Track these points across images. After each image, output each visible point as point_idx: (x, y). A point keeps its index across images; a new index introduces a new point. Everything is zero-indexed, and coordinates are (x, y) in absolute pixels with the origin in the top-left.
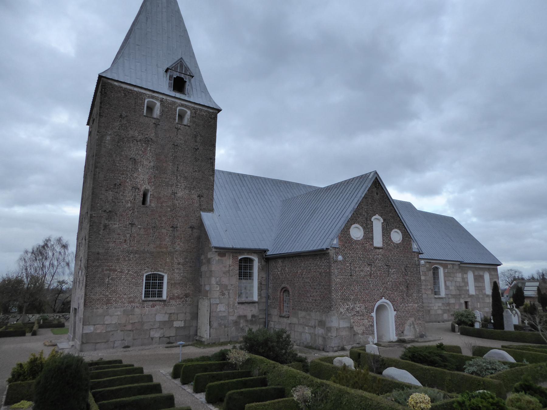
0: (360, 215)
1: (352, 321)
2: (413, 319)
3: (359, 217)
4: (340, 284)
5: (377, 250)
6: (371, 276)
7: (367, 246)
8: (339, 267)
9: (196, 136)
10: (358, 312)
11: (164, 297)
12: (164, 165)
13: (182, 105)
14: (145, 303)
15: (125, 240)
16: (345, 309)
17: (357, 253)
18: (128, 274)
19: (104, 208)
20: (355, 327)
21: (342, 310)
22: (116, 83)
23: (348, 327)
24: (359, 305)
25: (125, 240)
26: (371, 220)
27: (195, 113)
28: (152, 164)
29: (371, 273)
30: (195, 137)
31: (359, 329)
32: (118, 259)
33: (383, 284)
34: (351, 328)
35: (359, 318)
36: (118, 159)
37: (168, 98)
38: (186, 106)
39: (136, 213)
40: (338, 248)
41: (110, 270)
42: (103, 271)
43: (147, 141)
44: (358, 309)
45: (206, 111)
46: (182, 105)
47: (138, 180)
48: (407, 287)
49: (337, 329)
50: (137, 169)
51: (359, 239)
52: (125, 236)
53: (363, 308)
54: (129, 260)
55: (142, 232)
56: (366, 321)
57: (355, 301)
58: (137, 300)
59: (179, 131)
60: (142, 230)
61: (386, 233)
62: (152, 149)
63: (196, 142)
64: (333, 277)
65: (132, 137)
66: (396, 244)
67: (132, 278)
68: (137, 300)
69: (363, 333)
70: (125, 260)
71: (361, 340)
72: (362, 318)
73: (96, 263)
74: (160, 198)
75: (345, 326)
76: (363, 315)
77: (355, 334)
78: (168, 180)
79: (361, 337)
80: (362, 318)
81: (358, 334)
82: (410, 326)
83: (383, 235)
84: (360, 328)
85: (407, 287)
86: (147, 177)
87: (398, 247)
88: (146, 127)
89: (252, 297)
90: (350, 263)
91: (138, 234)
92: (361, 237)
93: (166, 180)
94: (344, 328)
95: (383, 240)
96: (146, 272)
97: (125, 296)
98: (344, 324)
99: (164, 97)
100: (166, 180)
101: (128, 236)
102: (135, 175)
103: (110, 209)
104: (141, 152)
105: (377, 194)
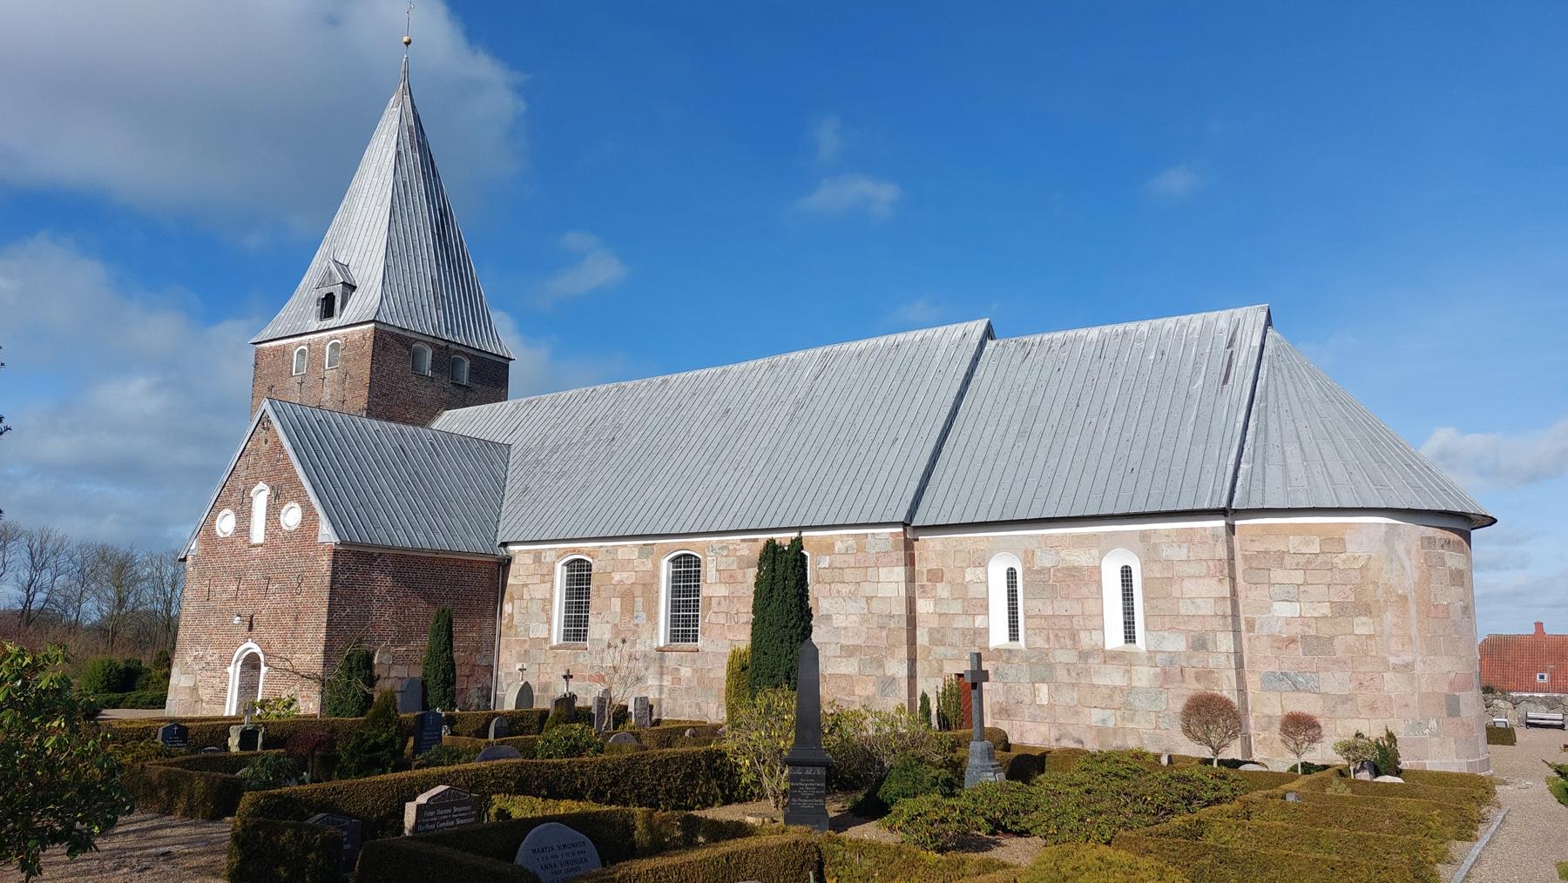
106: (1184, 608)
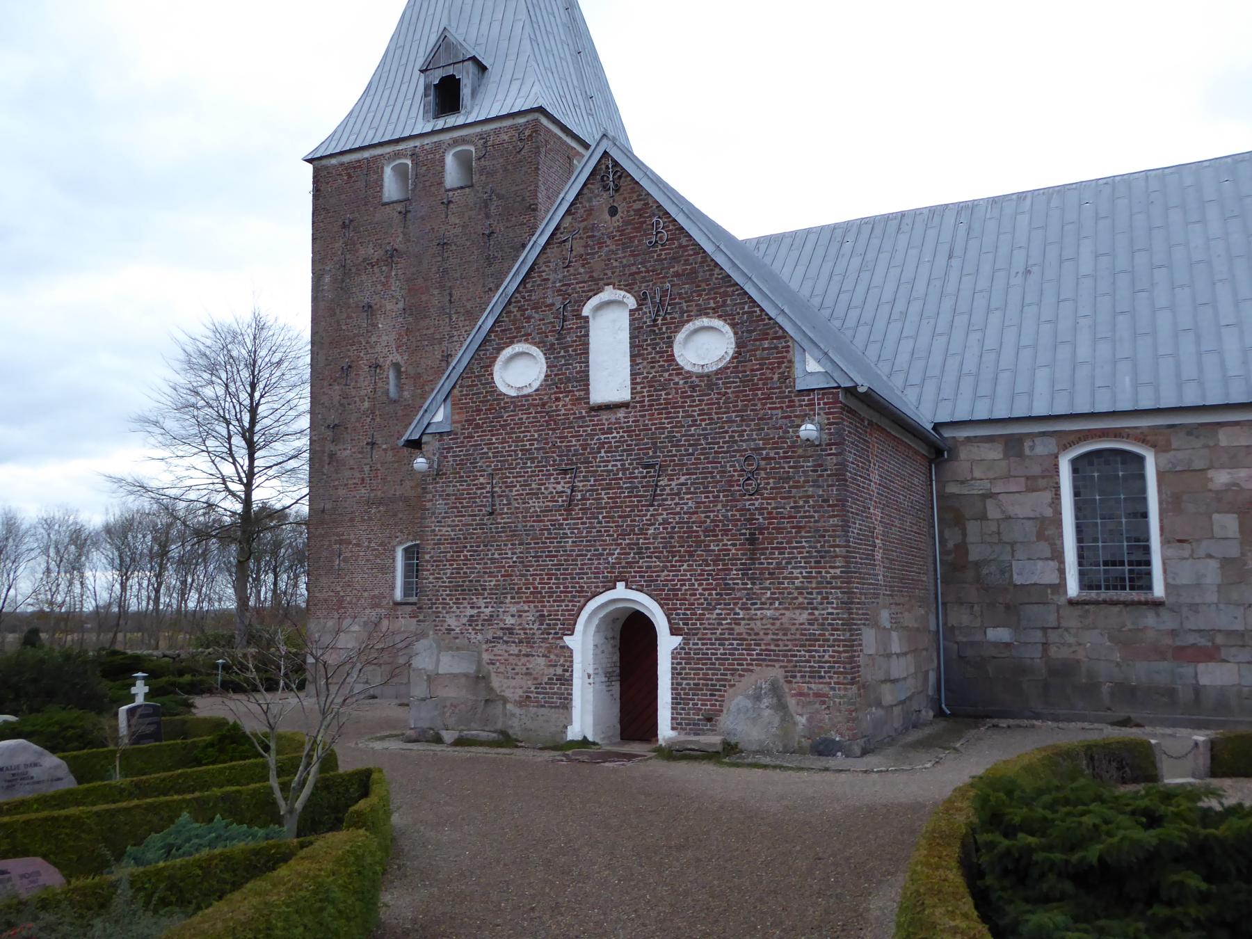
0: (536, 307)
1: (486, 657)
2: (777, 672)
3: (529, 319)
4: (453, 541)
5: (604, 416)
6: (569, 509)
7: (563, 406)
8: (450, 490)
9: (486, 204)
10: (510, 630)
11: (1159, 590)
12: (424, 298)
13: (456, 142)
14: (399, 608)
15: (363, 479)
16: (464, 620)
17: (518, 439)
18: (368, 547)
19: (328, 422)
20: (494, 678)
21: (451, 621)
22: (334, 161)
23: (466, 675)
24: (513, 609)
25: (363, 479)
26: (578, 316)
27: (485, 145)
28: (401, 305)
29: (571, 500)
30: (486, 207)
31: (509, 687)
32: (352, 520)
33: (623, 535)
34: (480, 679)
35: (514, 649)
36: (345, 316)
37: (426, 141)
38: (463, 140)
39: (378, 419)
40: (449, 433)
41: (341, 542)
42: (330, 546)
43: (392, 256)
44: (510, 621)
45: (510, 127)
46: (456, 142)
47: (378, 349)
48: (752, 540)
49: (429, 677)
50: (375, 326)
51: (525, 392)
52: (362, 471)
53: (530, 617)
54: (370, 519)
55: (390, 456)
56: (541, 661)
57: (498, 595)
58: (384, 602)
59: (451, 206)
60: (390, 453)
61: (650, 343)
62: (400, 272)
63: (488, 216)
64: (431, 523)
65: (365, 260)
66: (700, 376)
67: (377, 557)
68: (384, 602)
69: (525, 701)
70: (363, 520)
71: (515, 723)
72: (525, 650)
73: (320, 531)
74: (419, 376)
75: (456, 670)
76: (529, 641)
77: (492, 699)
78: (432, 330)
79: (517, 711)
80: (525, 650)
81: (505, 700)
82: (757, 698)
83: (633, 357)
84: (513, 683)
85: (752, 540)
86: (394, 336)
87: (710, 386)
88: (470, 211)
89: (1149, 587)
90: (492, 476)
91: (382, 464)
92: (536, 385)
93: (429, 332)
94: (455, 676)
95: (634, 375)
96: (400, 543)
97: (366, 594)
98: (449, 664)
99: (417, 143)
100: (429, 332)
101: (367, 469)
102: (374, 339)
103: (337, 422)
104: (379, 287)
105: (613, 211)
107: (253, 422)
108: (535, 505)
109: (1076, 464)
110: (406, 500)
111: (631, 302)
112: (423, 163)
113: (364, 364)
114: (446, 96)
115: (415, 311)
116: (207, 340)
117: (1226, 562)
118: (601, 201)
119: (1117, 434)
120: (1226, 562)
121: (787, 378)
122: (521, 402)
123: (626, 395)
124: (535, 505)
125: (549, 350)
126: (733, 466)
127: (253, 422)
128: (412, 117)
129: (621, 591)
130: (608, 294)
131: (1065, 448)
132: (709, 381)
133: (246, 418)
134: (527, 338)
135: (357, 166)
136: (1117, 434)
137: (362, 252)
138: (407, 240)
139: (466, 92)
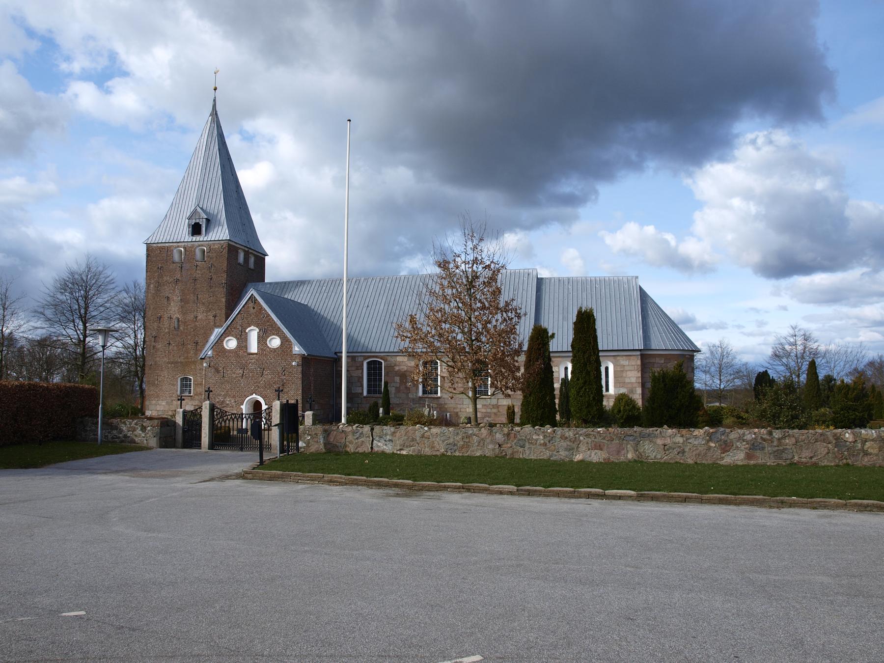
7: (241, 353)
61: (262, 340)
106: (627, 380)
107: (86, 313)
108: (234, 376)
109: (368, 363)
110: (181, 363)
111: (258, 330)
112: (189, 250)
113: (166, 316)
114: (196, 229)
115: (184, 301)
116: (65, 275)
117: (396, 388)
118: (251, 305)
119: (376, 357)
120: (396, 388)
121: (291, 351)
122: (230, 351)
123: (256, 351)
124: (234, 376)
125: (238, 339)
126: (280, 369)
127: (86, 313)
128: (183, 234)
129: (254, 396)
130: (252, 327)
131: (365, 359)
132: (275, 350)
133: (83, 311)
134: (232, 336)
135: (163, 248)
136: (376, 357)
137: (165, 278)
138: (181, 276)
139: (204, 229)
